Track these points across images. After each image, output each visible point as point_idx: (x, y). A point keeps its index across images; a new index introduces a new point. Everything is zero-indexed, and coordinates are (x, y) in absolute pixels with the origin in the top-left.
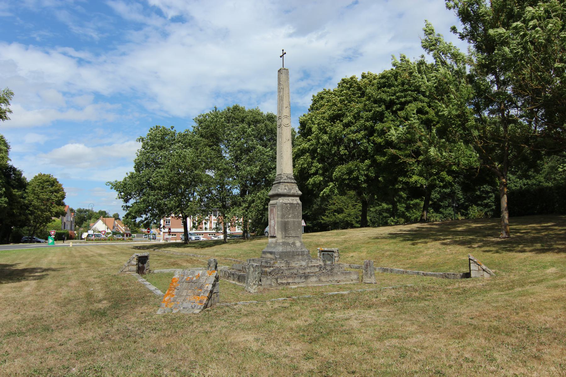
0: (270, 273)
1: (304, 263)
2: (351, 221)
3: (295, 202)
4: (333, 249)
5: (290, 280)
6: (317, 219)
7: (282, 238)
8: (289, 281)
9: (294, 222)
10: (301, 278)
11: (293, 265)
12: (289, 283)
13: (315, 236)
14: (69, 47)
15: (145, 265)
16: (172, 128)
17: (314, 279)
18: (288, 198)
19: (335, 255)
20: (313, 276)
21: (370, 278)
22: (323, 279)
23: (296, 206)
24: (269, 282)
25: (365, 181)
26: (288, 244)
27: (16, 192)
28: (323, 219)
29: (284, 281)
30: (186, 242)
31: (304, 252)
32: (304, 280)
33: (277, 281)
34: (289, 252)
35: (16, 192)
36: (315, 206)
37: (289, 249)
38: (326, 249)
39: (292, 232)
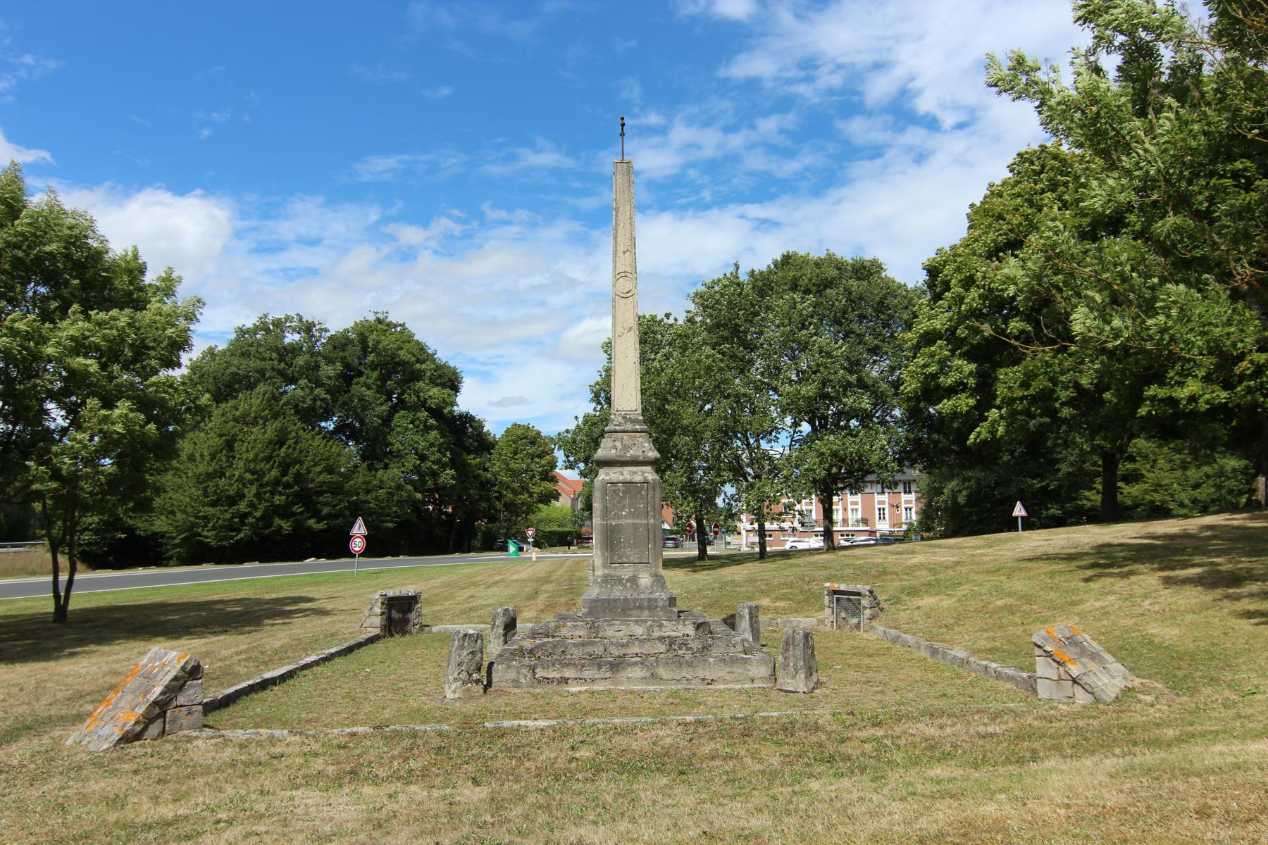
0: (531, 652)
1: (639, 631)
2: (1163, 502)
3: (638, 478)
4: (860, 587)
5: (569, 673)
6: (1076, 499)
7: (604, 566)
8: (567, 675)
9: (635, 526)
10: (600, 667)
11: (609, 632)
12: (566, 681)
13: (940, 546)
14: (180, 188)
15: (412, 616)
16: (667, 316)
17: (637, 672)
18: (620, 469)
19: (865, 602)
20: (635, 664)
21: (794, 677)
22: (662, 672)
23: (641, 488)
24: (511, 675)
25: (1070, 403)
26: (619, 580)
27: (472, 460)
28: (1087, 499)
29: (556, 675)
30: (763, 555)
31: (656, 600)
32: (608, 675)
33: (534, 673)
34: (615, 600)
35: (472, 460)
36: (1064, 468)
37: (617, 592)
38: (843, 587)
39: (628, 551)
